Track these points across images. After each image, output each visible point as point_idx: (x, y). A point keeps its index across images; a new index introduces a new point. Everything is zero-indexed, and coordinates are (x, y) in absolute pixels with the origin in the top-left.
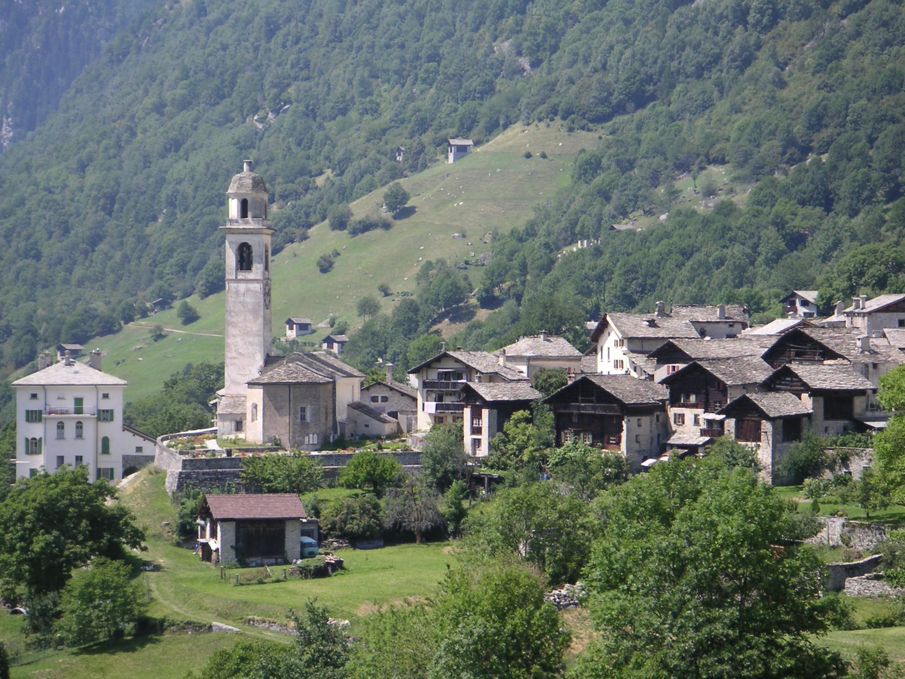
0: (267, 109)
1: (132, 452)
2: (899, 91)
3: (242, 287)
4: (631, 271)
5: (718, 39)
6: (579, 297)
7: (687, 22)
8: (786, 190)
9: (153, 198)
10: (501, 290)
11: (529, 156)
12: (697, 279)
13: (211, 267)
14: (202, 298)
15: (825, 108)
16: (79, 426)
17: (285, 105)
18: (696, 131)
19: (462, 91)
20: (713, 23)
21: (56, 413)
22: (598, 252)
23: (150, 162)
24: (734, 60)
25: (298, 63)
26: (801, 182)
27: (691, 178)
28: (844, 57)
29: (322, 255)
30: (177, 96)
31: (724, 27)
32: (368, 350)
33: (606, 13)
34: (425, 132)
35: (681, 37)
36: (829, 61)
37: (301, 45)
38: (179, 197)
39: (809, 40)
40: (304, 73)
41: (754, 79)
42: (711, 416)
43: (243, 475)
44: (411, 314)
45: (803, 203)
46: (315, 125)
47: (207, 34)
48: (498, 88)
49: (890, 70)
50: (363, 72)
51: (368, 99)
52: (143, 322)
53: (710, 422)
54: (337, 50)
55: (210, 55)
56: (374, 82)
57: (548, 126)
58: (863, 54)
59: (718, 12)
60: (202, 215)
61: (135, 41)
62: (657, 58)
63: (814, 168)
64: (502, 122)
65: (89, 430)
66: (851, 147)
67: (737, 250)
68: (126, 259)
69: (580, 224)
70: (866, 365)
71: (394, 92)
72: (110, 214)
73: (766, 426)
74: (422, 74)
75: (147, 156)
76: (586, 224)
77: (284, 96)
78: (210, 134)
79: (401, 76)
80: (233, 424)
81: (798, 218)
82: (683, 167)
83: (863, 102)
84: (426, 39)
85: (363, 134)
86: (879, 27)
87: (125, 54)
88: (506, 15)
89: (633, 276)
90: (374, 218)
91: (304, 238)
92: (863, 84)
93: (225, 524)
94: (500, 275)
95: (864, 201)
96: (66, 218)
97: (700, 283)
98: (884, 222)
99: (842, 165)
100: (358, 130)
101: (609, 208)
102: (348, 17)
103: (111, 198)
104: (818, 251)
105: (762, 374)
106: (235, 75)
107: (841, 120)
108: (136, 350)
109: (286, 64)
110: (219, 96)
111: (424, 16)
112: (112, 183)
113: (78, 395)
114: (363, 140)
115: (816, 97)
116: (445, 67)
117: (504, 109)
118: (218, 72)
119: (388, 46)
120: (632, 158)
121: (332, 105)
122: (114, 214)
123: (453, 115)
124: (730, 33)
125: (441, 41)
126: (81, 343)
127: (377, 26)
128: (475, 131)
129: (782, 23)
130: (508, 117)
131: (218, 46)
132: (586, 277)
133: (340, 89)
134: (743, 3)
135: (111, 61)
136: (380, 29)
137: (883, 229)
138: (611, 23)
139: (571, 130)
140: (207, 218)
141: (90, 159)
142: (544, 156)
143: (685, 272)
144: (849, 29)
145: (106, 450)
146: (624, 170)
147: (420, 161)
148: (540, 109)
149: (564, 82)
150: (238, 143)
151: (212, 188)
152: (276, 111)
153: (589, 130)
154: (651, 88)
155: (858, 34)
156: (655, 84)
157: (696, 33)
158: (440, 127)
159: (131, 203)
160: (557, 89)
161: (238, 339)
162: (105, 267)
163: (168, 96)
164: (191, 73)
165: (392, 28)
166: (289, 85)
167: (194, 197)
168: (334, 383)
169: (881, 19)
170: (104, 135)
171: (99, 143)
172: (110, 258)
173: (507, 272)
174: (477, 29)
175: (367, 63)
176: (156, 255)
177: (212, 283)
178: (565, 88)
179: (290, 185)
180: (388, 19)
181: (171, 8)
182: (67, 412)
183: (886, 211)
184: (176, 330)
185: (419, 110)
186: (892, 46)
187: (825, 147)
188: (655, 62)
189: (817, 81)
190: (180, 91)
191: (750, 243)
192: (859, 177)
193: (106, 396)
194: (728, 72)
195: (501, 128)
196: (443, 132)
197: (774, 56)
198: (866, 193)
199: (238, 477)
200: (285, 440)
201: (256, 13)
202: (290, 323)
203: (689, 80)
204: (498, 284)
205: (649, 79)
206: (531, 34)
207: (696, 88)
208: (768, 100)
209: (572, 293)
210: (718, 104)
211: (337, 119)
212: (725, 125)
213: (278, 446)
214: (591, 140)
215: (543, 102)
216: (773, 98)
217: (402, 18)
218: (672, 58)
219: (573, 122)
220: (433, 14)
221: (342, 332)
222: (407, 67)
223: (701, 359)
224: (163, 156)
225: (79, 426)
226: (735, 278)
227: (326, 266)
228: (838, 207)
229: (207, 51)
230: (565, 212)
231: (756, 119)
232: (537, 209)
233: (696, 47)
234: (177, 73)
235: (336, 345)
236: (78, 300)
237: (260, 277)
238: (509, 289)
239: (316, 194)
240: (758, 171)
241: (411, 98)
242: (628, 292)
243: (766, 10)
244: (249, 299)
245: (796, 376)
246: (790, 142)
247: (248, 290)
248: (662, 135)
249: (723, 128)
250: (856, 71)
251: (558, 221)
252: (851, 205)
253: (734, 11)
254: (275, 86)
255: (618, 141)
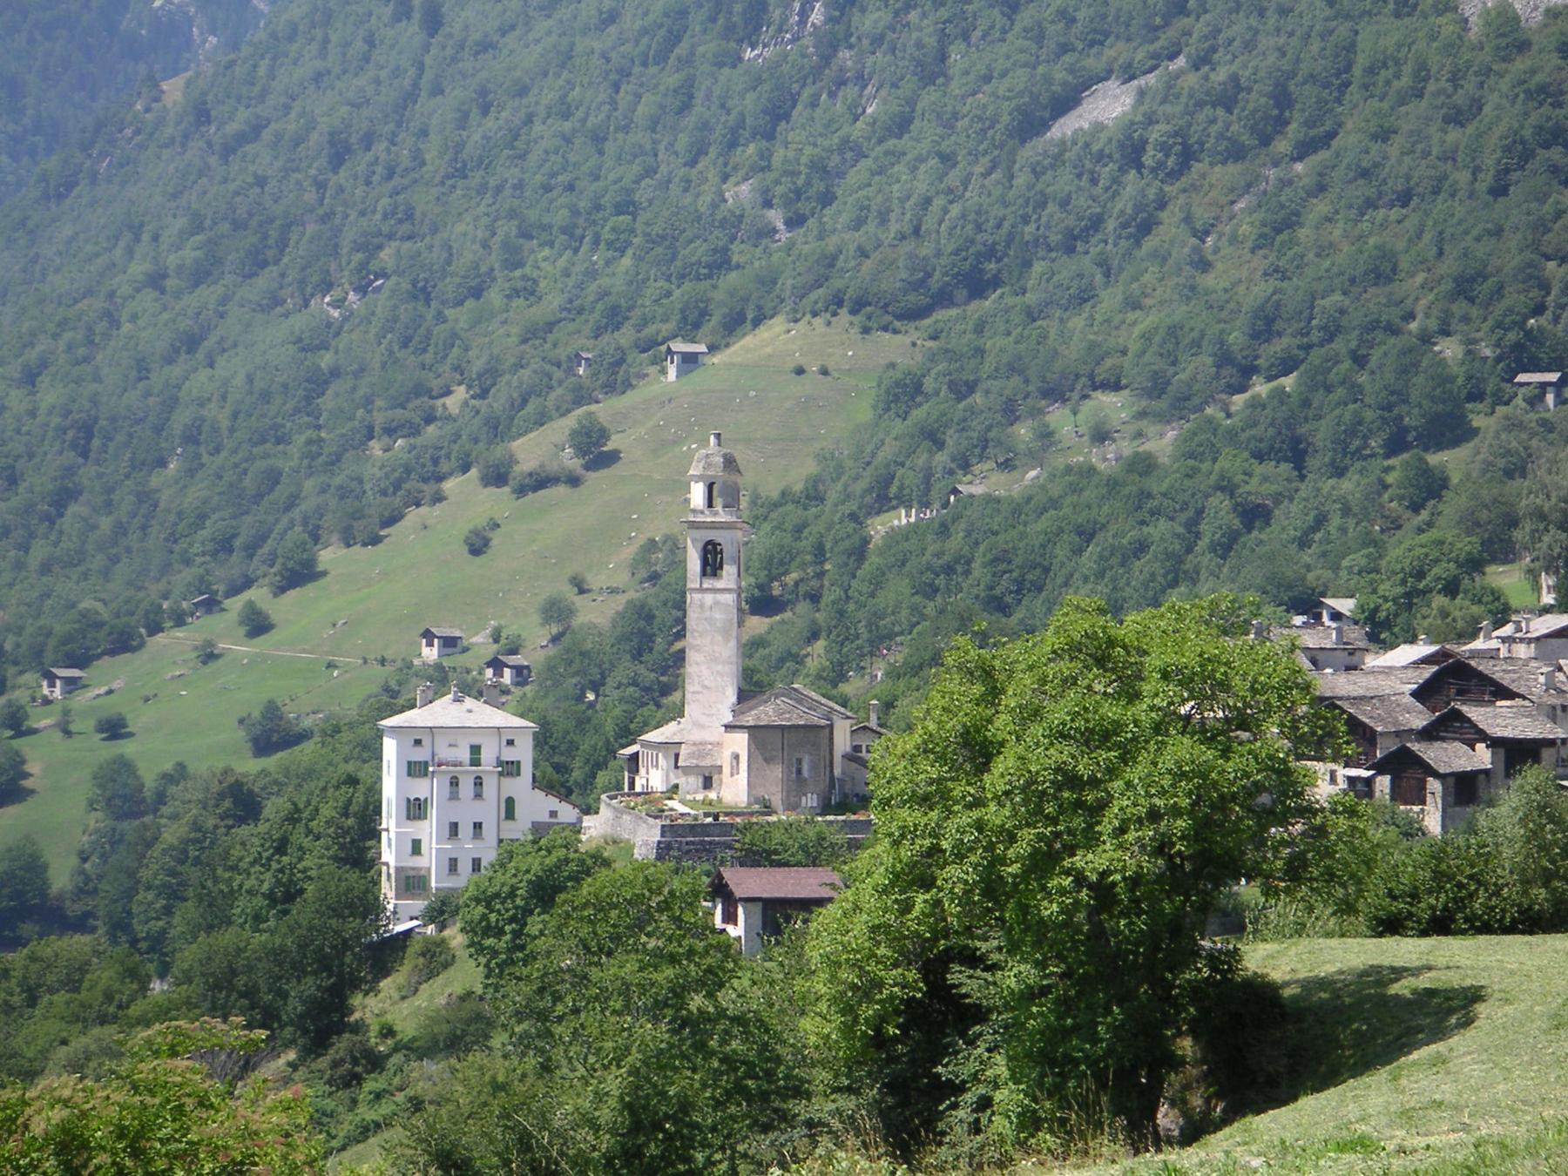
0: (347, 286)
1: (544, 817)
2: (1391, 280)
3: (709, 598)
4: (1000, 559)
5: (1098, 190)
6: (918, 599)
7: (1046, 162)
8: (1232, 435)
9: (158, 430)
10: (784, 586)
11: (800, 371)
12: (1109, 574)
13: (290, 545)
14: (275, 595)
15: (1278, 305)
16: (478, 782)
17: (376, 279)
18: (1074, 334)
19: (679, 263)
20: (1088, 165)
21: (447, 764)
22: (944, 530)
23: (148, 371)
24: (1124, 226)
25: (394, 213)
26: (1255, 424)
27: (1067, 411)
28: (1301, 225)
29: (471, 526)
30: (188, 262)
31: (1106, 171)
32: (574, 680)
33: (911, 143)
34: (618, 328)
35: (1039, 187)
36: (1279, 231)
37: (396, 181)
38: (206, 428)
39: (1241, 196)
40: (405, 228)
41: (1161, 257)
42: (1354, 772)
43: (738, 845)
44: (642, 624)
45: (1260, 456)
46: (430, 315)
47: (225, 161)
48: (735, 259)
49: (1376, 247)
50: (507, 229)
51: (518, 273)
52: (179, 633)
53: (1352, 781)
54: (459, 192)
55: (237, 193)
56: (528, 245)
57: (829, 324)
58: (1329, 220)
59: (1095, 148)
60: (251, 459)
61: (88, 163)
62: (1004, 218)
63: (1276, 402)
64: (750, 316)
65: (490, 786)
66: (1330, 370)
67: (1160, 530)
68: (121, 529)
69: (896, 482)
70: (1554, 708)
71: (562, 262)
72: (85, 455)
73: (1434, 785)
74: (606, 234)
75: (143, 360)
76: (907, 482)
77: (374, 265)
78: (248, 325)
79: (572, 236)
80: (701, 780)
81: (1255, 481)
82: (1055, 393)
83: (1337, 297)
84: (612, 176)
85: (515, 330)
86: (1355, 179)
87: (71, 186)
88: (742, 141)
89: (1004, 566)
90: (553, 467)
91: (438, 498)
92: (1335, 269)
93: (749, 905)
94: (781, 563)
95: (1353, 454)
96: (10, 461)
97: (1114, 580)
98: (1386, 487)
99: (1318, 398)
100: (505, 322)
101: (942, 458)
102: (477, 137)
103: (87, 429)
104: (1292, 532)
105: (1419, 718)
106: (286, 228)
107: (1302, 324)
108: (173, 678)
109: (374, 212)
110: (257, 262)
111: (605, 139)
112: (87, 405)
113: (475, 741)
114: (514, 340)
115: (1262, 290)
116: (647, 224)
117: (755, 294)
118: (254, 223)
119: (547, 188)
120: (972, 378)
121: (458, 280)
122: (92, 455)
123: (664, 301)
124: (1115, 181)
125: (637, 182)
126: (81, 667)
127: (526, 153)
128: (706, 328)
129: (1197, 167)
130: (760, 308)
131: (251, 180)
132: (929, 568)
133: (468, 257)
134: (1136, 135)
135: (47, 197)
136: (533, 159)
137: (1386, 497)
138: (921, 159)
139: (866, 330)
140: (260, 465)
141: (44, 364)
142: (825, 372)
143: (1089, 560)
144: (1306, 181)
145: (510, 814)
146: (960, 397)
147: (620, 377)
148: (813, 296)
149: (851, 253)
150: (300, 340)
151: (264, 416)
152: (362, 290)
153: (895, 332)
154: (992, 266)
155: (1321, 188)
156: (999, 260)
157: (1063, 181)
158: (645, 322)
159: (120, 438)
160: (840, 264)
161: (703, 668)
162: (84, 543)
163: (172, 260)
164: (207, 223)
165: (553, 158)
166: (380, 247)
167: (232, 430)
168: (831, 726)
169: (1358, 166)
170: (63, 324)
171: (55, 336)
172: (95, 527)
173: (792, 559)
174: (693, 163)
175: (512, 214)
176: (176, 524)
177: (291, 570)
178: (853, 263)
179: (399, 411)
180: (544, 144)
181: (148, 110)
182: (460, 764)
183: (1387, 470)
184: (239, 648)
185: (607, 294)
186: (1376, 208)
187: (1287, 366)
188: (999, 226)
189: (1260, 262)
190: (190, 253)
191: (1183, 517)
192: (1347, 417)
193: (510, 743)
194: (1115, 245)
195: (748, 325)
196: (650, 330)
197: (1188, 219)
198: (1357, 443)
199: (731, 848)
200: (777, 801)
201: (311, 125)
202: (428, 636)
203: (1054, 255)
204: (777, 578)
205: (991, 253)
206: (786, 173)
207: (1067, 268)
208: (1186, 291)
209: (908, 591)
210: (1103, 294)
211: (467, 304)
212: (1117, 328)
213: (768, 809)
214: (901, 348)
215: (818, 284)
216: (1193, 288)
217: (568, 140)
218: (1026, 220)
219: (869, 318)
220: (620, 136)
221: (514, 652)
222: (581, 221)
223: (1340, 699)
224: (169, 361)
225: (478, 782)
226: (1167, 573)
227: (478, 546)
228: (1313, 463)
229: (232, 187)
230: (868, 464)
231: (1169, 321)
232: (821, 458)
233: (1065, 203)
234: (182, 222)
235: (507, 672)
236: (47, 595)
237: (733, 586)
238: (797, 584)
239: (449, 428)
240: (1182, 405)
241: (592, 274)
242: (998, 591)
243: (1172, 147)
244: (718, 615)
245: (1469, 720)
246: (1224, 359)
247: (717, 603)
248: (1016, 343)
249: (1114, 333)
250: (1322, 248)
251: (857, 478)
252: (1333, 461)
253: (1122, 146)
254: (358, 248)
255: (947, 351)
